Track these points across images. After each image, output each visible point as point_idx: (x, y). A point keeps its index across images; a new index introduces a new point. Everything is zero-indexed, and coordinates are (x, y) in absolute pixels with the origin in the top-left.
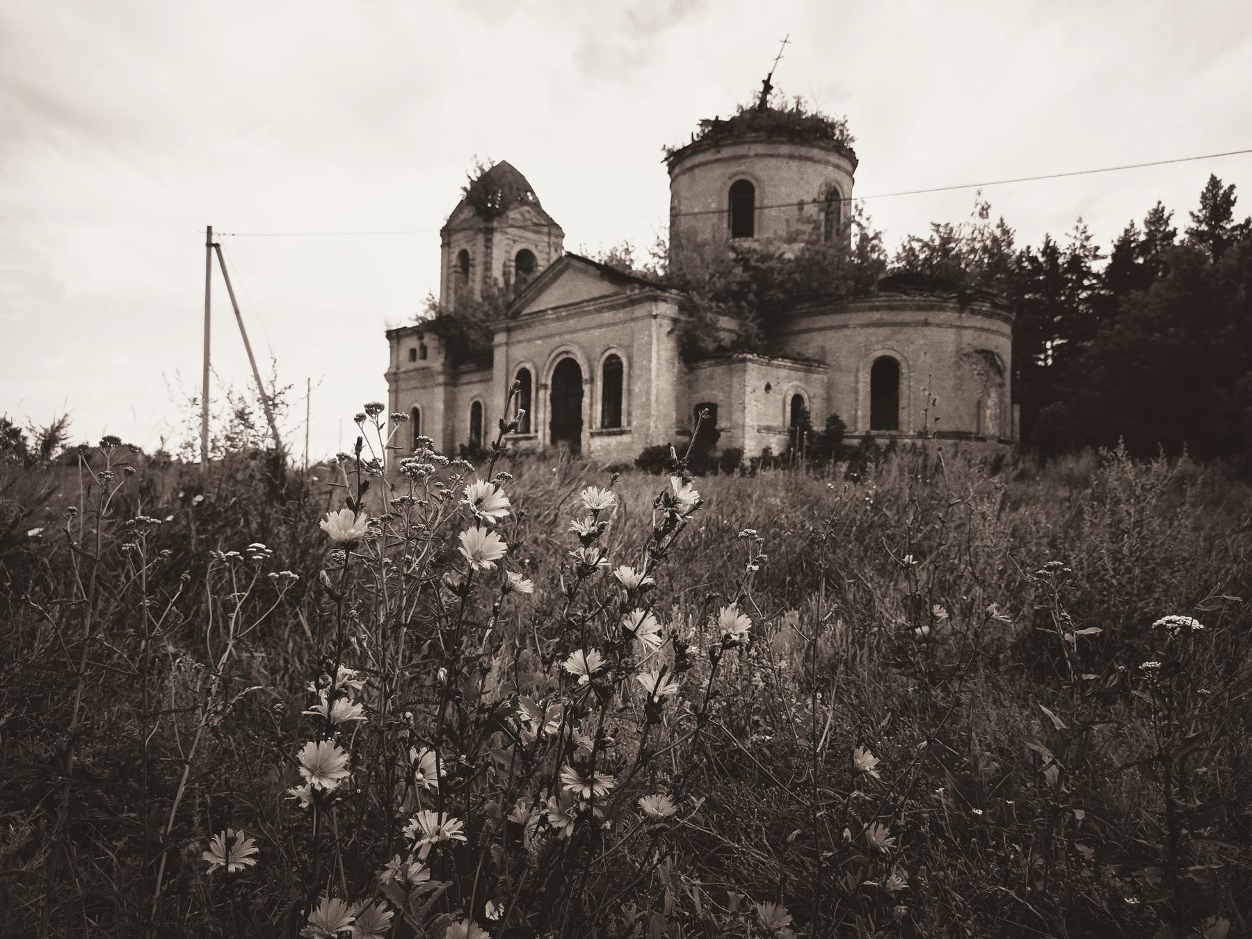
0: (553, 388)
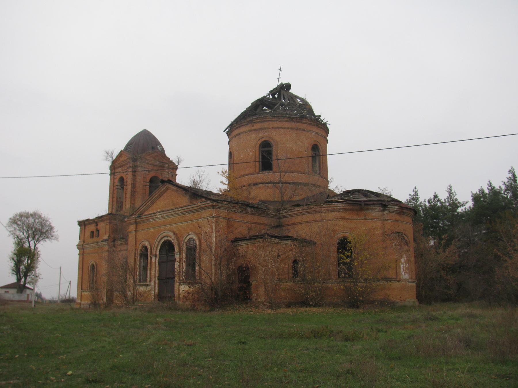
0: (160, 258)
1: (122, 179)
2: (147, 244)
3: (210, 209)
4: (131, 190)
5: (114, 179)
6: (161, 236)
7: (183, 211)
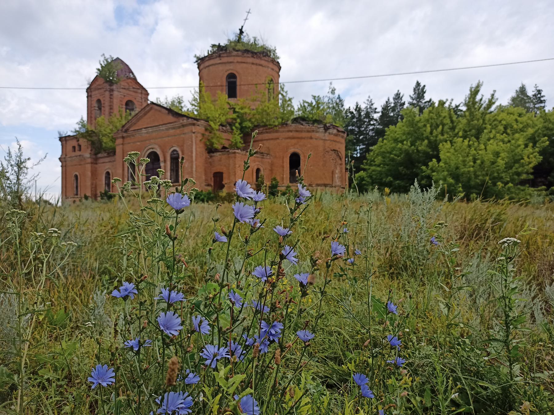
1: (99, 101)
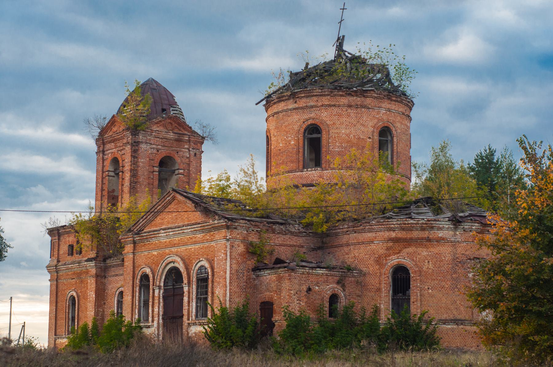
1: (115, 161)
2: (148, 271)
3: (223, 230)
4: (131, 180)
5: (103, 160)
6: (166, 261)
7: (192, 230)
